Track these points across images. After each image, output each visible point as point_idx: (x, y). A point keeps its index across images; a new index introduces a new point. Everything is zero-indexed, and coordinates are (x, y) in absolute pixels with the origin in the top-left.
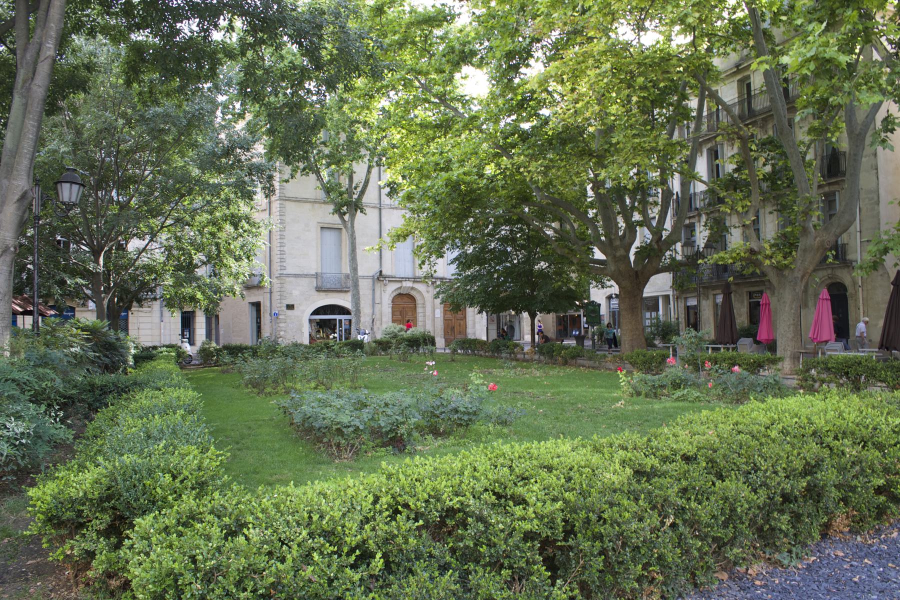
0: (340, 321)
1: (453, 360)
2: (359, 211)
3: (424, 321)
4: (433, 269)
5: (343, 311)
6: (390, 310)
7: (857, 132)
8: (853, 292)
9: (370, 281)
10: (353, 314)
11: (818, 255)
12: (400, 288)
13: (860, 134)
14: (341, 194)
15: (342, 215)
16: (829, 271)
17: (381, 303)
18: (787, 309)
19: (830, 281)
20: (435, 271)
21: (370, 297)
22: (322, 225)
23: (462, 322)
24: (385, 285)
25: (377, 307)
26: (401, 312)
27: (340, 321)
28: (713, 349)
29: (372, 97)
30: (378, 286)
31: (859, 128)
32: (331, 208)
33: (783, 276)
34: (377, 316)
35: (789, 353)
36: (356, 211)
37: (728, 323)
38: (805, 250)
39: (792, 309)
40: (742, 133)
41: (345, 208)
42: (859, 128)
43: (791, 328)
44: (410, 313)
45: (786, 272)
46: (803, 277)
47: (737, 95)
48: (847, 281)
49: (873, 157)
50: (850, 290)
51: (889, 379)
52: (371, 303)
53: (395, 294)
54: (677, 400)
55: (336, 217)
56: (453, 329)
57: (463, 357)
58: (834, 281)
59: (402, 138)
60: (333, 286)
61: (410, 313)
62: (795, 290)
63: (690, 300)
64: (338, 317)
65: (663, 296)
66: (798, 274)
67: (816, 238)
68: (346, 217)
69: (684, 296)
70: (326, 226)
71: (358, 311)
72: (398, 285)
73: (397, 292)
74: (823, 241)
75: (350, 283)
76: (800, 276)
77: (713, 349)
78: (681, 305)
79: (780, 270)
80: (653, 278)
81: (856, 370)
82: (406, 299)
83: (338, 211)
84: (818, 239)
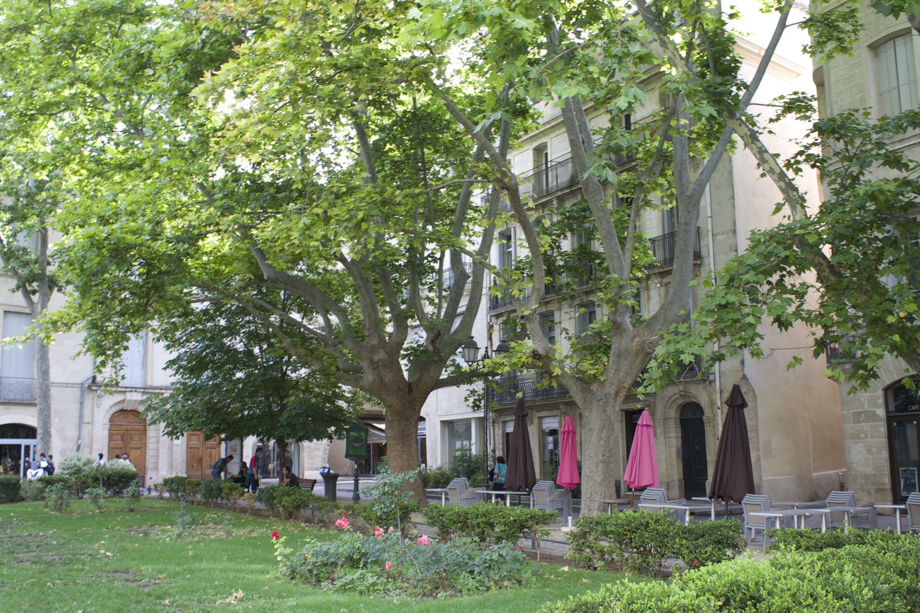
0: (27, 448)
1: (132, 510)
2: (56, 289)
3: (158, 449)
4: (121, 373)
5: (28, 432)
6: (106, 433)
7: (689, 193)
8: (711, 415)
9: (77, 392)
10: (39, 437)
11: (638, 361)
12: (123, 401)
13: (692, 196)
14: (26, 264)
15: (28, 294)
16: (681, 387)
17: (91, 423)
18: (594, 438)
19: (682, 401)
20: (123, 378)
21: (76, 413)
22: (7, 309)
23: (214, 452)
24: (100, 397)
25: (86, 429)
26: (123, 436)
27: (27, 448)
28: (497, 496)
29: (32, 118)
30: (89, 398)
31: (691, 187)
32: (13, 283)
33: (590, 392)
34: (85, 441)
35: (597, 504)
36: (51, 289)
37: (521, 459)
38: (619, 356)
39: (600, 439)
40: (506, 180)
41: (35, 284)
42: (691, 187)
43: (600, 468)
44: (137, 438)
45: (594, 387)
46: (617, 394)
47: (569, 150)
48: (704, 401)
49: (731, 235)
50: (707, 413)
51: (685, 551)
52: (76, 421)
53: (114, 410)
54: (344, 589)
55: (20, 294)
56: (200, 460)
57: (173, 505)
58: (687, 400)
59: (80, 181)
60: (19, 397)
61: (137, 438)
62: (605, 411)
63: (546, 420)
64: (23, 442)
65: (476, 418)
66: (611, 390)
67: (634, 337)
68: (35, 298)
69: (502, 419)
70: (12, 309)
71: (47, 434)
72: (118, 398)
73: (118, 408)
74: (644, 342)
75: (37, 393)
76: (612, 392)
77: (497, 496)
78: (499, 431)
79: (587, 383)
80: (432, 393)
81: (641, 536)
82: (131, 418)
83: (23, 286)
84: (637, 339)
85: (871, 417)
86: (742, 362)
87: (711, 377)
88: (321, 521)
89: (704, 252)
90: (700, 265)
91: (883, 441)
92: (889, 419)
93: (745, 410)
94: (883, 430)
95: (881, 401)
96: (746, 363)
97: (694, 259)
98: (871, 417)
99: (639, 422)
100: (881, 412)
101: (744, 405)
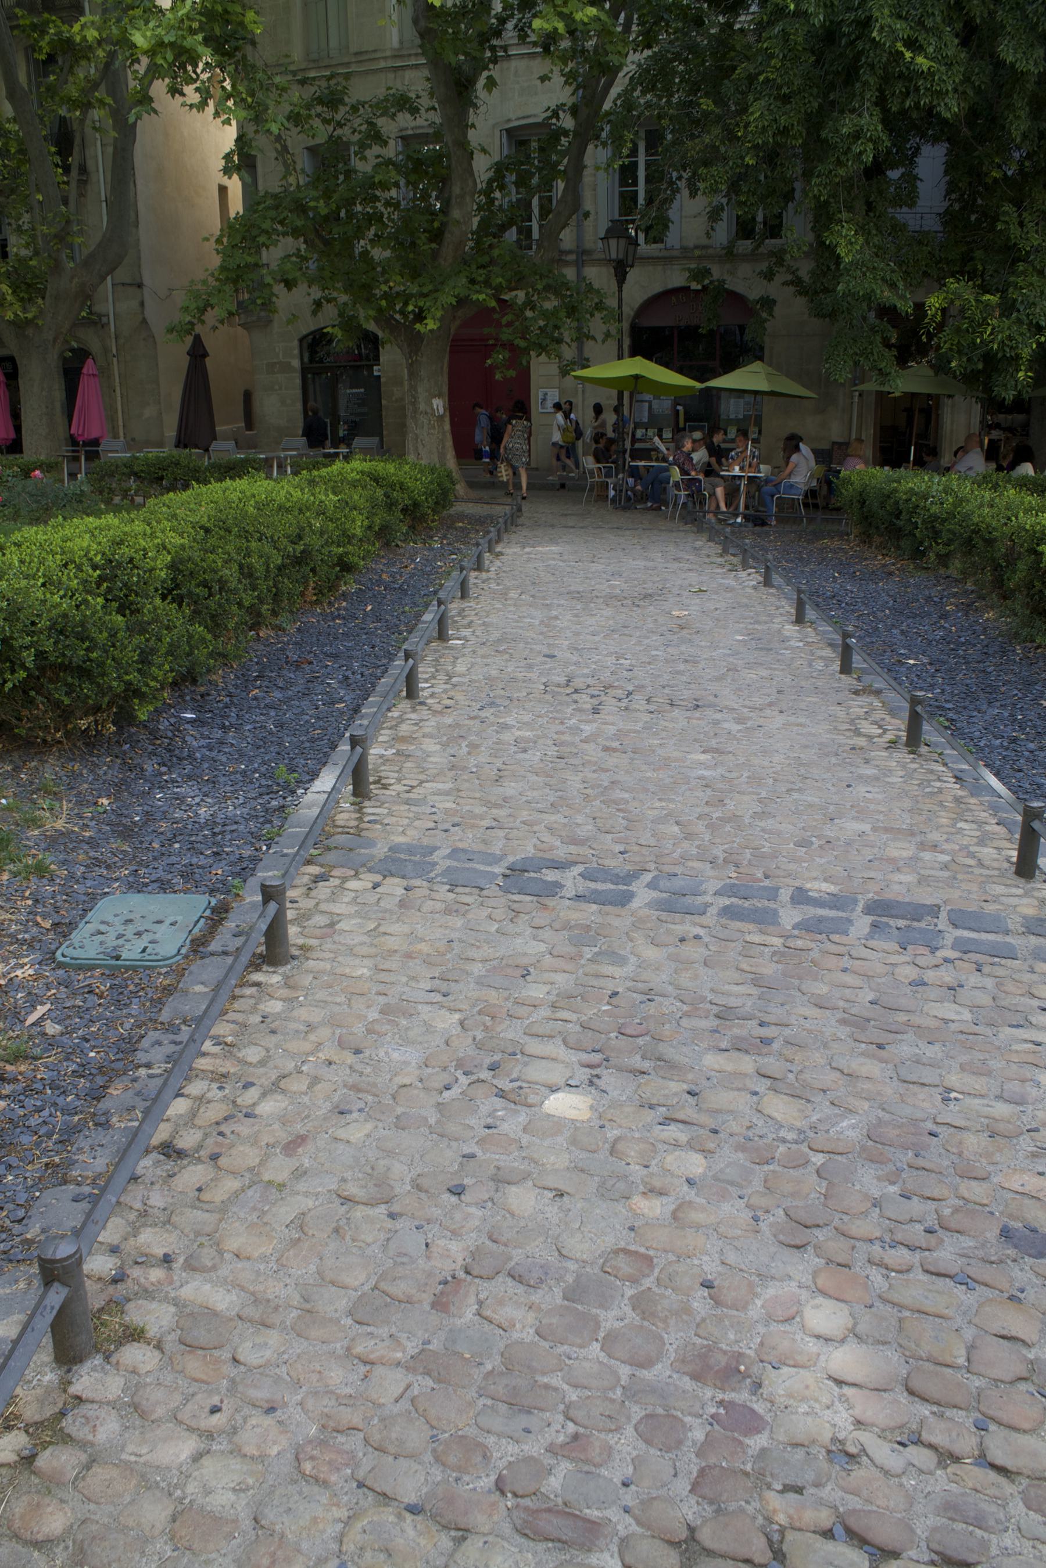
45: (30, 332)
46: (55, 340)
84: (76, 280)
85: (286, 367)
86: (142, 304)
87: (104, 320)
88: (288, 510)
89: (90, 164)
90: (85, 182)
91: (298, 392)
92: (304, 370)
93: (207, 359)
94: (298, 381)
95: (296, 352)
96: (146, 304)
97: (621, 186)
98: (286, 367)
99: (85, 371)
100: (296, 363)
101: (205, 355)
